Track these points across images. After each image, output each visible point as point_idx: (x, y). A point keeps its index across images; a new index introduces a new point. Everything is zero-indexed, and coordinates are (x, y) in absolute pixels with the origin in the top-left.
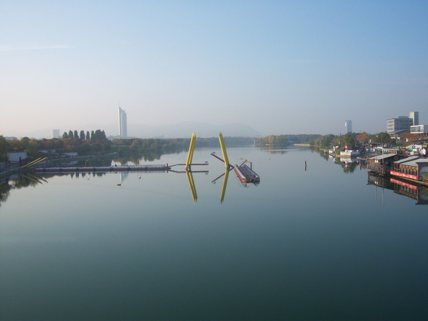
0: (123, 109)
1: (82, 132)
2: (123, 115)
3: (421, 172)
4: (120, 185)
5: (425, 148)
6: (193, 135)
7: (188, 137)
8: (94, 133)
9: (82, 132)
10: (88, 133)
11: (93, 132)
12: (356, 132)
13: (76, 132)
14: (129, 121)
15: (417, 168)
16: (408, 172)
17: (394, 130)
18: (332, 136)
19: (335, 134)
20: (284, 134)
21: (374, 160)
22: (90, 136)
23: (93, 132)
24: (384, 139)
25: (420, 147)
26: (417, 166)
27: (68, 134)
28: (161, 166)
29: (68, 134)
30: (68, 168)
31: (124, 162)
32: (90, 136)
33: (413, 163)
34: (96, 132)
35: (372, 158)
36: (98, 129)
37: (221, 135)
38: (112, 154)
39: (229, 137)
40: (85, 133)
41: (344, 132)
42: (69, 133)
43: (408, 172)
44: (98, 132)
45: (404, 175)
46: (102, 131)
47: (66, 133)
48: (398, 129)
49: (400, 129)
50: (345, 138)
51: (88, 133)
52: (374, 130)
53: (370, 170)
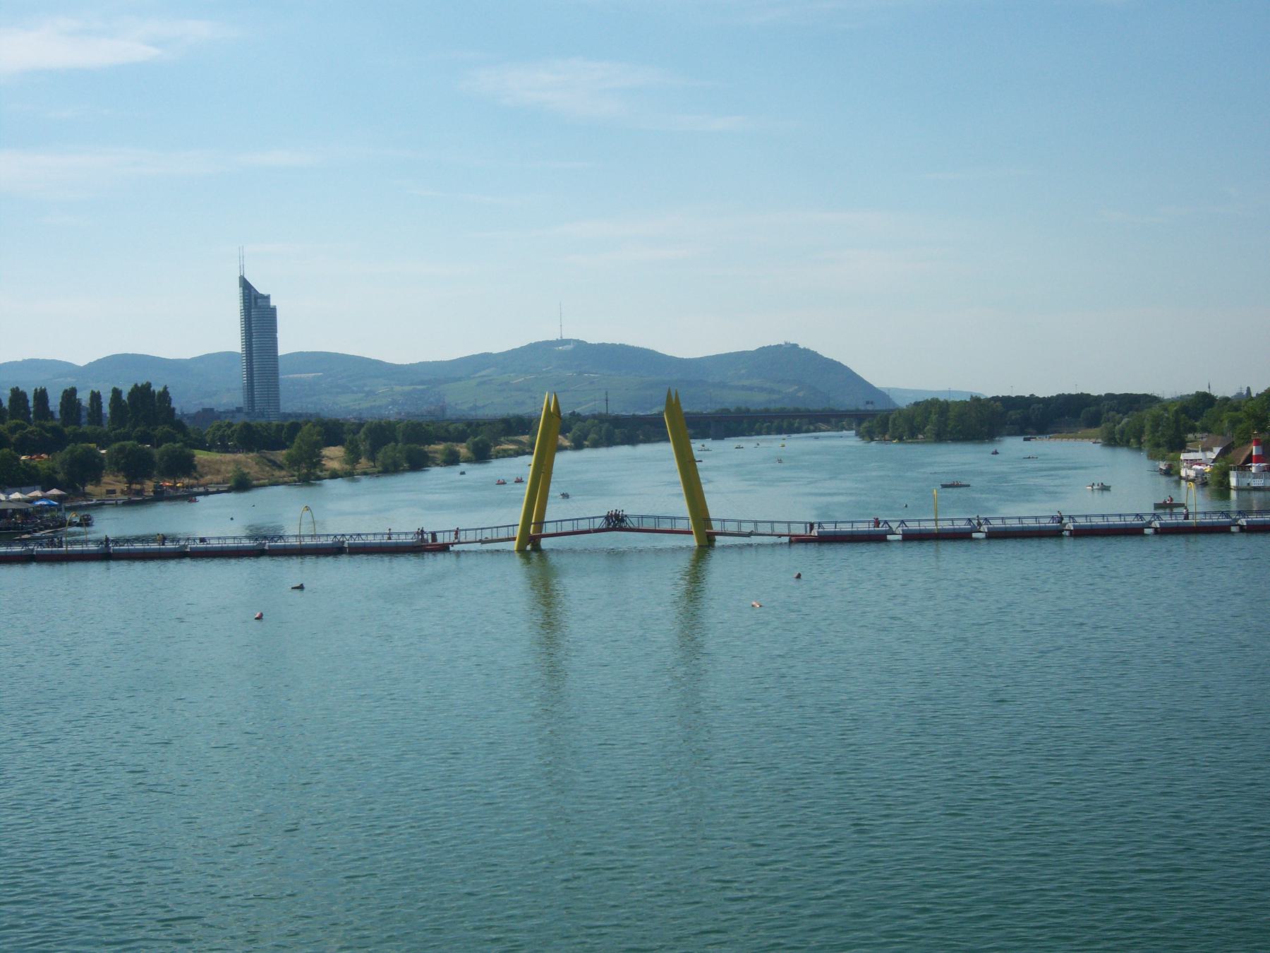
1: (70, 395)
2: (258, 314)
4: (301, 587)
6: (546, 400)
8: (125, 397)
9: (70, 395)
10: (96, 397)
11: (116, 393)
13: (41, 396)
14: (289, 342)
18: (1204, 401)
19: (1219, 392)
22: (106, 409)
23: (116, 393)
31: (44, 490)
32: (106, 409)
34: (131, 394)
38: (418, 447)
39: (739, 410)
40: (84, 397)
42: (11, 401)
46: (157, 388)
51: (96, 397)
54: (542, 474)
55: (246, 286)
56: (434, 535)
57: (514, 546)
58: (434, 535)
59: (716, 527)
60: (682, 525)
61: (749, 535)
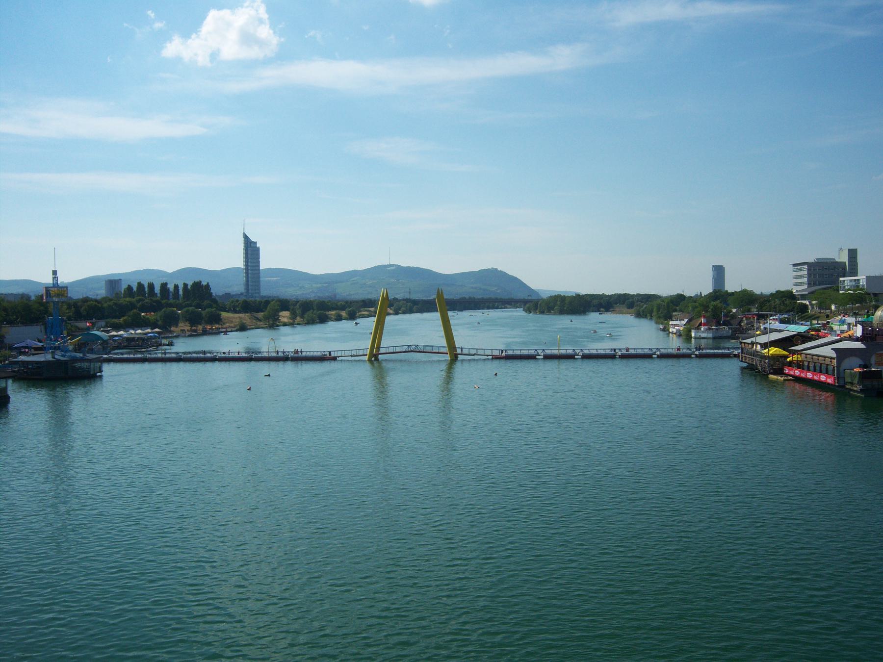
0: (253, 239)
3: (841, 369)
5: (862, 323)
6: (382, 292)
7: (372, 296)
8: (189, 287)
10: (176, 287)
11: (185, 285)
12: (729, 291)
15: (835, 361)
16: (818, 369)
17: (806, 287)
18: (681, 298)
19: (687, 294)
20: (642, 293)
21: (752, 343)
22: (181, 292)
23: (185, 285)
24: (785, 304)
25: (851, 320)
26: (834, 355)
27: (135, 289)
28: (319, 354)
29: (135, 289)
30: (720, 351)
32: (181, 292)
33: (828, 351)
35: (749, 341)
36: (197, 280)
37: (440, 294)
39: (470, 298)
40: (171, 287)
41: (706, 288)
43: (818, 369)
44: (197, 285)
45: (809, 375)
46: (204, 283)
47: (130, 288)
48: (815, 284)
49: (819, 285)
50: (659, 301)
51: (176, 287)
52: (763, 286)
53: (745, 365)
54: (380, 325)
55: (246, 237)
56: (330, 352)
57: (366, 358)
58: (330, 352)
59: (459, 351)
60: (443, 350)
61: (474, 355)
